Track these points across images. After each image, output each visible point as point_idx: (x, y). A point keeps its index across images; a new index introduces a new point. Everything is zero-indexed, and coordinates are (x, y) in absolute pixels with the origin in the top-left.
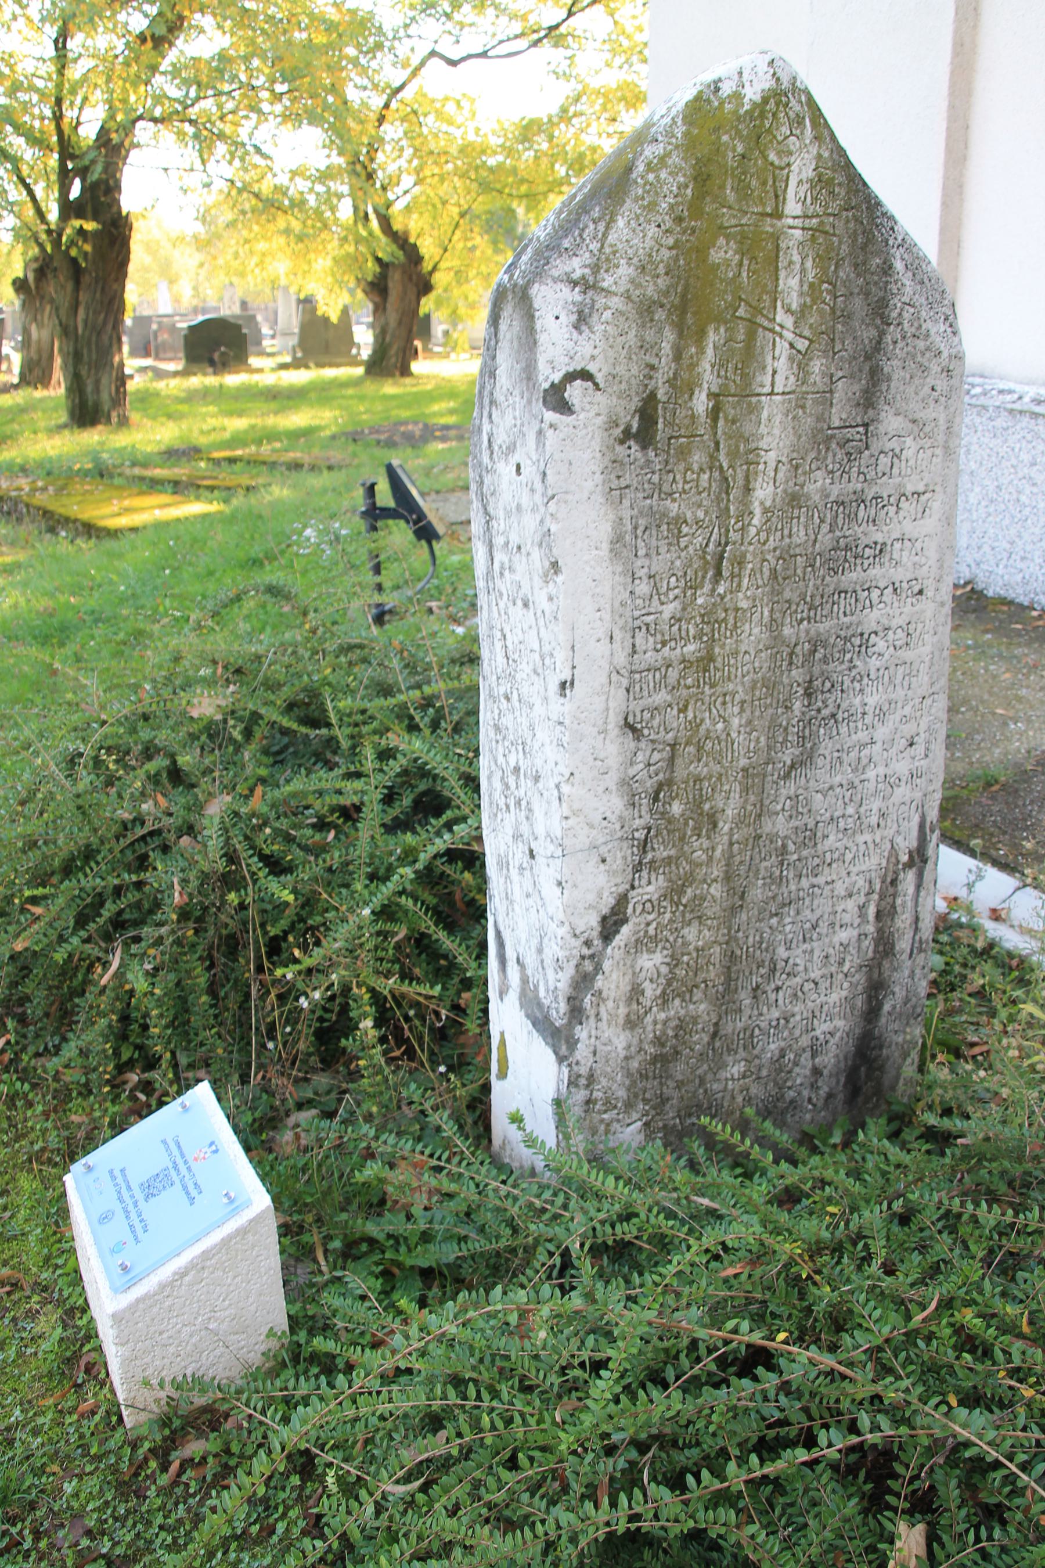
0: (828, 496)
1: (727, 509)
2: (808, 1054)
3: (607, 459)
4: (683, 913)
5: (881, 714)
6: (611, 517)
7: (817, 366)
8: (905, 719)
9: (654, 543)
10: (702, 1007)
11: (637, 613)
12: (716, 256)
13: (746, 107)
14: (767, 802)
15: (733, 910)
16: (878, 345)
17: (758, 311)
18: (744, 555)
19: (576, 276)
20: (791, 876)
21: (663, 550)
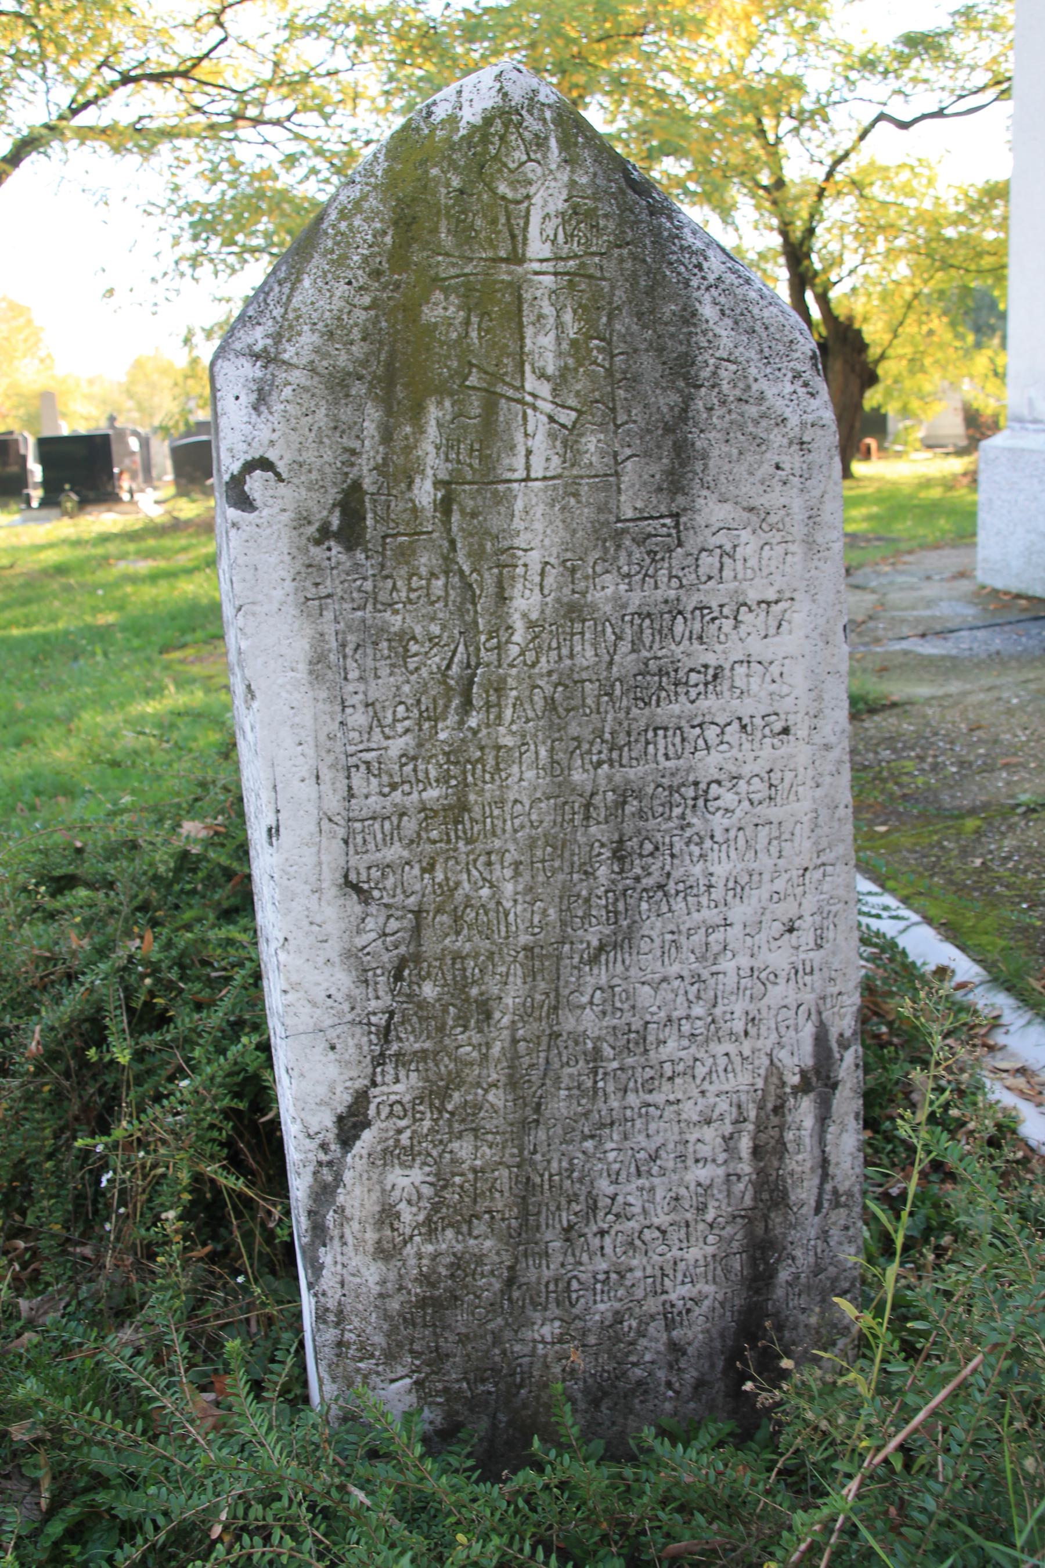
0: (624, 606)
1: (475, 623)
2: (660, 1323)
4: (449, 1121)
5: (737, 888)
6: (309, 632)
7: (591, 443)
8: (777, 897)
9: (370, 663)
10: (488, 1244)
11: (351, 749)
12: (431, 314)
13: (463, 132)
14: (565, 992)
15: (525, 1126)
16: (683, 414)
18: (503, 680)
19: (257, 348)
20: (611, 1088)
21: (384, 672)
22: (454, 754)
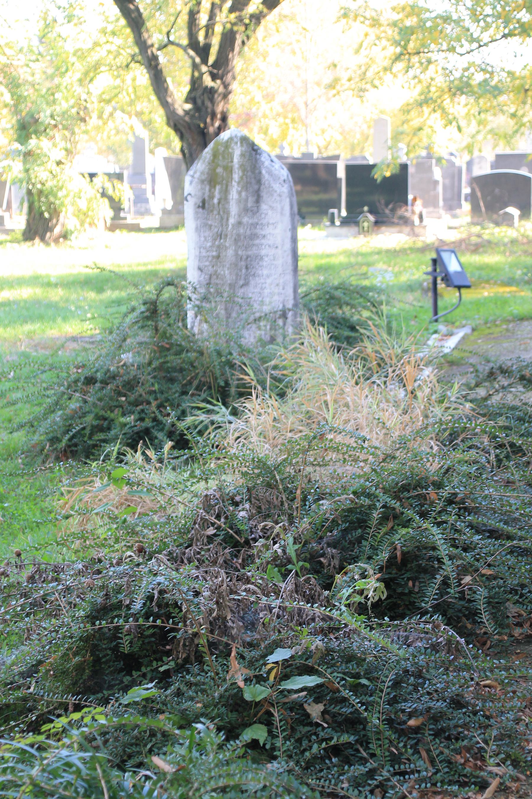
5: (268, 276)
7: (243, 194)
22: (219, 247)
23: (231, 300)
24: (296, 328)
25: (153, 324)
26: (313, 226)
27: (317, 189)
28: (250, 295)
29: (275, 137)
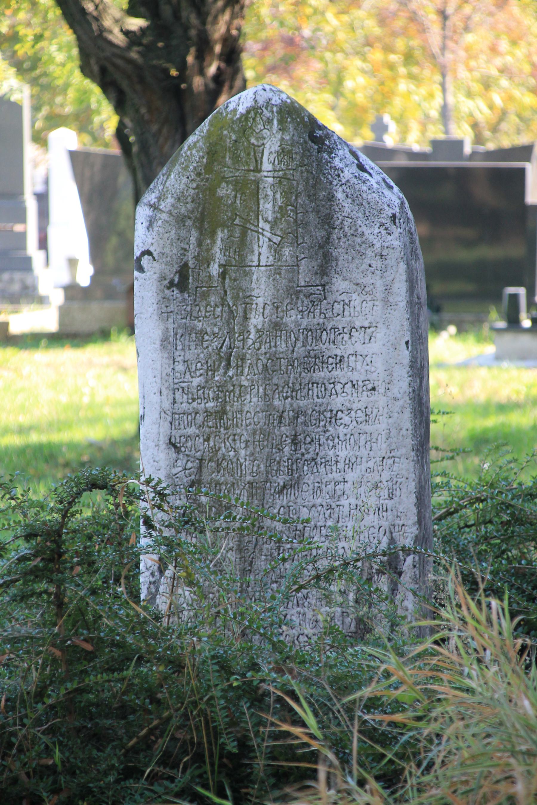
0: (300, 325)
3: (160, 296)
5: (350, 464)
6: (162, 327)
7: (287, 251)
9: (187, 343)
11: (176, 381)
13: (238, 116)
16: (328, 240)
17: (248, 221)
18: (245, 355)
19: (152, 203)
21: (193, 347)
22: (221, 387)
23: (254, 525)
24: (426, 599)
25: (52, 589)
26: (461, 330)
27: (469, 233)
28: (304, 513)
29: (360, 98)
